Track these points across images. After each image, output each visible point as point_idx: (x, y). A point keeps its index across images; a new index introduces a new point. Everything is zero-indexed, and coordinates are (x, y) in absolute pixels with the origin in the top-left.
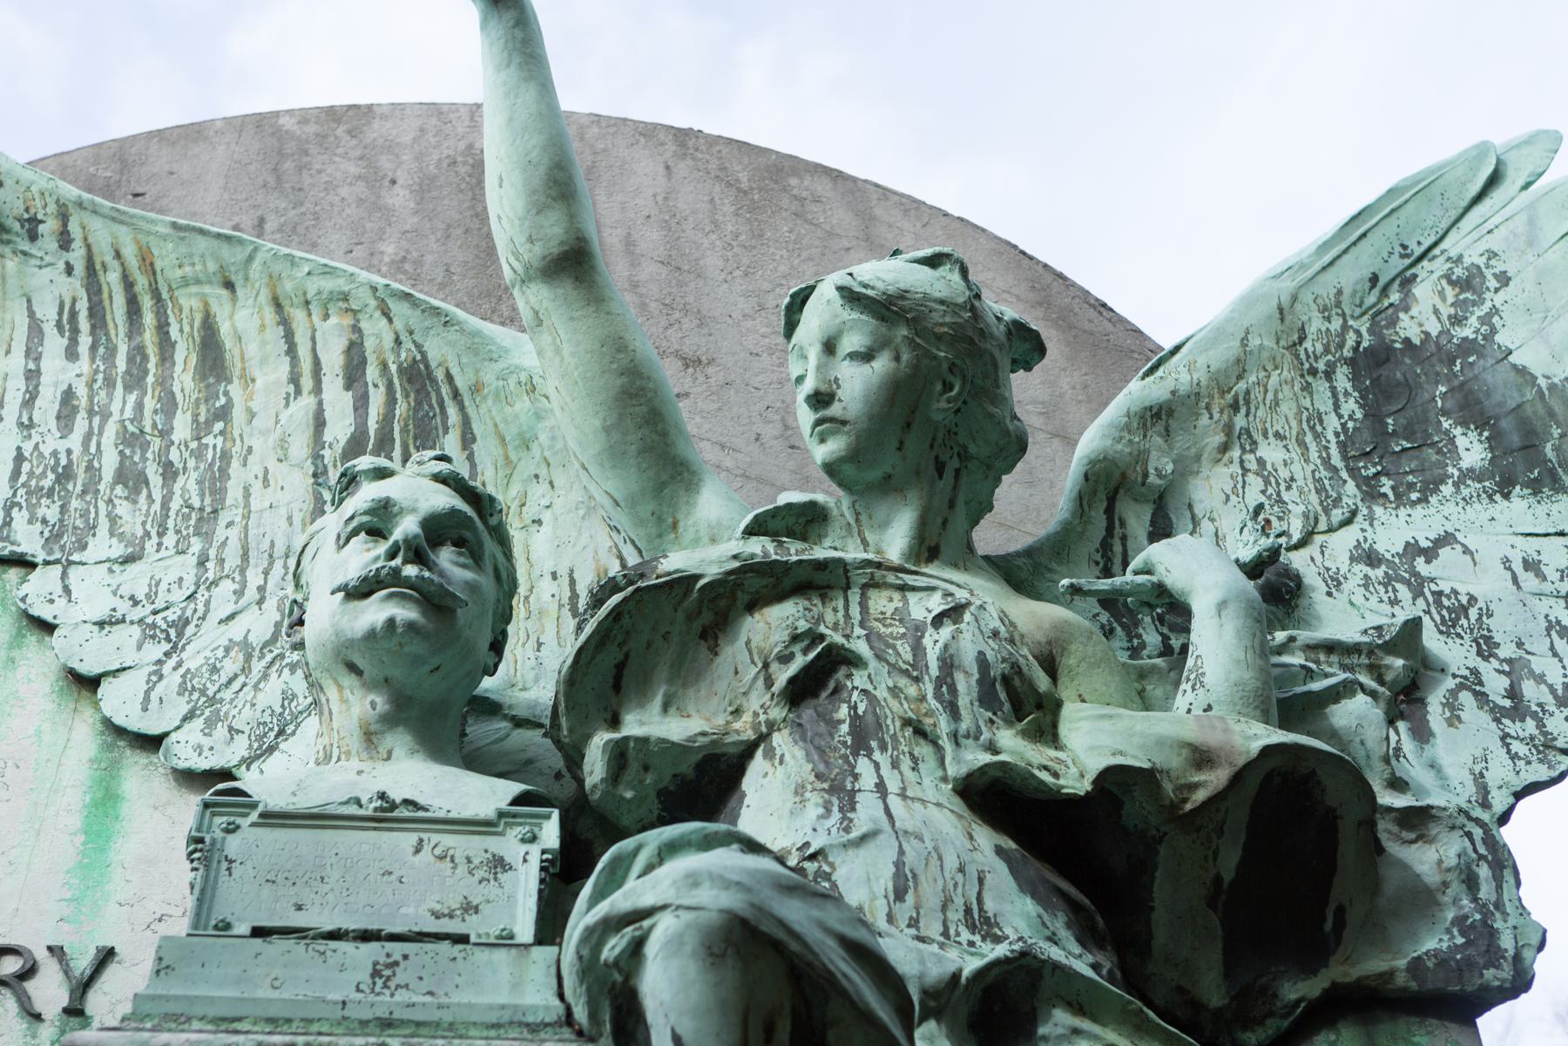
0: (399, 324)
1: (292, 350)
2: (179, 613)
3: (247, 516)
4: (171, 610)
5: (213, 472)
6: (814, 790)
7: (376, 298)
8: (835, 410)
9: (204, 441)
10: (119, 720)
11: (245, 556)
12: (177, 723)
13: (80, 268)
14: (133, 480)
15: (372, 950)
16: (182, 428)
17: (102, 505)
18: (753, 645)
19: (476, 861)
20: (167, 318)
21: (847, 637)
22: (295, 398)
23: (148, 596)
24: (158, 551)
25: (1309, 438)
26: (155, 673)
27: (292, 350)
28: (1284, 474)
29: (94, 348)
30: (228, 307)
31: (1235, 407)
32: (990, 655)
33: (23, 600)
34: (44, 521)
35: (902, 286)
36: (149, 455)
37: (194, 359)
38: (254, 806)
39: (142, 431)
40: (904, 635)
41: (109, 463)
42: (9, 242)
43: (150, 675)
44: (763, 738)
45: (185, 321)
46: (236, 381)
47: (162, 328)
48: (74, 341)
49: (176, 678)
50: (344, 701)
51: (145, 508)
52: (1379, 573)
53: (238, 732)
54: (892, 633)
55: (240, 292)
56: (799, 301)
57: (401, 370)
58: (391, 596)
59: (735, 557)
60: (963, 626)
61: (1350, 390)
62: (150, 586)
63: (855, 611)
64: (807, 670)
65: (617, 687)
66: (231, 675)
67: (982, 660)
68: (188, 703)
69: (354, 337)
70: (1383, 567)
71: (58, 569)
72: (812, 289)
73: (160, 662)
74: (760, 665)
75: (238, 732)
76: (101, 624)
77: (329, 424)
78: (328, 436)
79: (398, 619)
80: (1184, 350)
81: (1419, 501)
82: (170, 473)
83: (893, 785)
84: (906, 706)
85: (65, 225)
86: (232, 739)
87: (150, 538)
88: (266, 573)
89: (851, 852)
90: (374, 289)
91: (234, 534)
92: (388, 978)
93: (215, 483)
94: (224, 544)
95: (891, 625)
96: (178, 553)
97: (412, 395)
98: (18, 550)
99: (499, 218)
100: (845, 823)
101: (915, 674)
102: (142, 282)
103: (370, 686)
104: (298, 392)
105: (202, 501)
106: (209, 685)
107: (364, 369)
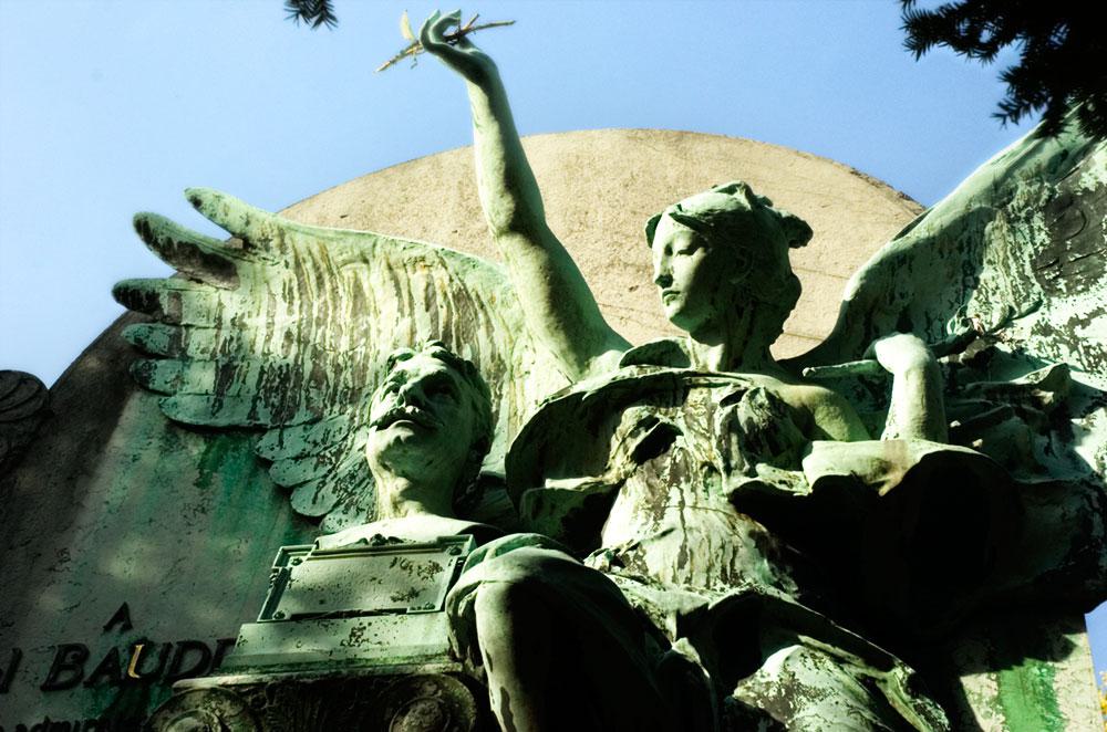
0: (450, 270)
1: (399, 294)
8: (673, 287)
12: (330, 509)
13: (292, 263)
17: (303, 393)
19: (423, 568)
21: (672, 418)
25: (1011, 260)
28: (992, 285)
30: (366, 273)
31: (961, 249)
32: (756, 419)
33: (258, 450)
34: (273, 405)
42: (255, 254)
44: (622, 483)
46: (372, 314)
47: (334, 290)
48: (291, 303)
49: (333, 484)
52: (1050, 339)
55: (371, 264)
56: (653, 225)
57: (454, 296)
58: (398, 426)
60: (740, 404)
61: (1042, 227)
70: (1053, 335)
72: (660, 217)
73: (325, 476)
79: (402, 438)
80: (925, 219)
81: (1083, 290)
83: (689, 501)
85: (283, 240)
89: (656, 542)
92: (359, 637)
96: (340, 414)
101: (708, 435)
102: (323, 266)
104: (403, 315)
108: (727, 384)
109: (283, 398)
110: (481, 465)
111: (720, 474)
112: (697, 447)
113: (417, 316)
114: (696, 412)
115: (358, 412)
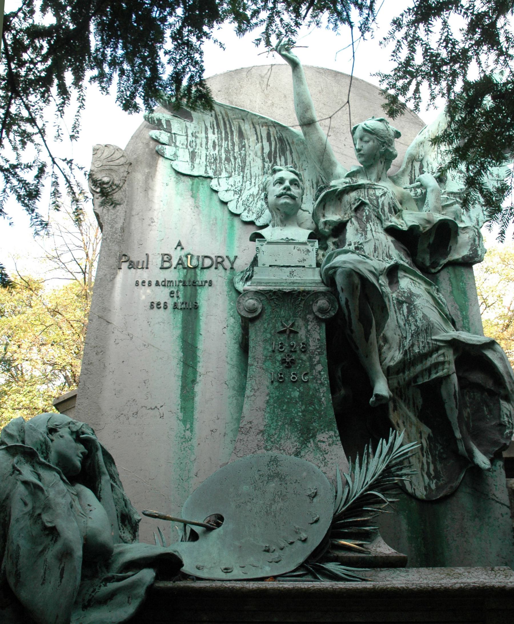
1: (256, 134)
3: (250, 168)
8: (362, 152)
10: (232, 211)
11: (251, 176)
14: (228, 159)
15: (289, 269)
16: (236, 149)
27: (256, 134)
29: (218, 132)
30: (243, 124)
35: (375, 127)
37: (237, 134)
38: (266, 240)
41: (223, 156)
47: (231, 128)
48: (214, 131)
50: (276, 215)
58: (285, 198)
63: (366, 193)
67: (389, 204)
71: (217, 179)
73: (238, 199)
76: (226, 191)
78: (265, 152)
83: (373, 230)
88: (255, 179)
91: (248, 171)
93: (244, 160)
94: (247, 174)
98: (209, 175)
102: (226, 119)
104: (258, 142)
109: (216, 167)
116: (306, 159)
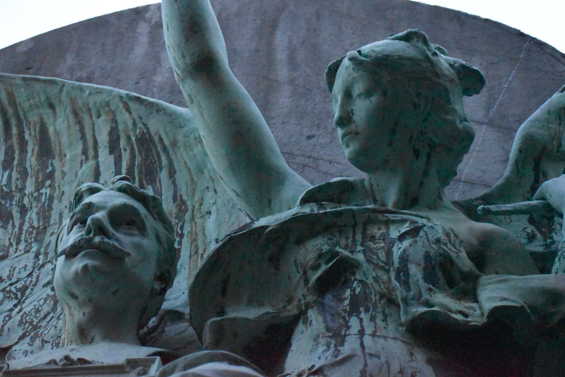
0: (135, 115)
1: (83, 137)
2: (23, 283)
4: (20, 282)
5: (45, 207)
6: (324, 337)
7: (123, 102)
9: (41, 192)
12: (16, 340)
18: (298, 262)
20: (24, 129)
21: (352, 252)
22: (85, 162)
23: (8, 276)
24: (16, 252)
26: (8, 316)
27: (83, 137)
35: (386, 53)
36: (14, 203)
37: (37, 149)
39: (11, 191)
40: (383, 247)
43: (5, 317)
45: (32, 129)
46: (57, 157)
49: (19, 317)
51: (10, 231)
53: (46, 342)
54: (377, 247)
55: (58, 110)
57: (137, 140)
59: (88, 186)
60: (418, 238)
62: (10, 271)
63: (359, 237)
64: (327, 273)
65: (224, 293)
66: (46, 313)
68: (23, 329)
69: (114, 125)
73: (11, 310)
74: (302, 273)
75: (46, 342)
77: (102, 174)
79: (90, 265)
82: (23, 210)
83: (368, 330)
84: (382, 286)
86: (43, 346)
87: (12, 246)
90: (121, 97)
91: (53, 239)
94: (49, 244)
95: (378, 243)
97: (144, 153)
99: (169, 47)
100: (336, 352)
103: (81, 306)
105: (39, 223)
106: (34, 319)
107: (119, 142)
108: (404, 221)
110: (163, 300)
111: (399, 306)
112: (376, 279)
113: (101, 159)
114: (375, 246)
115: (42, 250)
116: (211, 185)
